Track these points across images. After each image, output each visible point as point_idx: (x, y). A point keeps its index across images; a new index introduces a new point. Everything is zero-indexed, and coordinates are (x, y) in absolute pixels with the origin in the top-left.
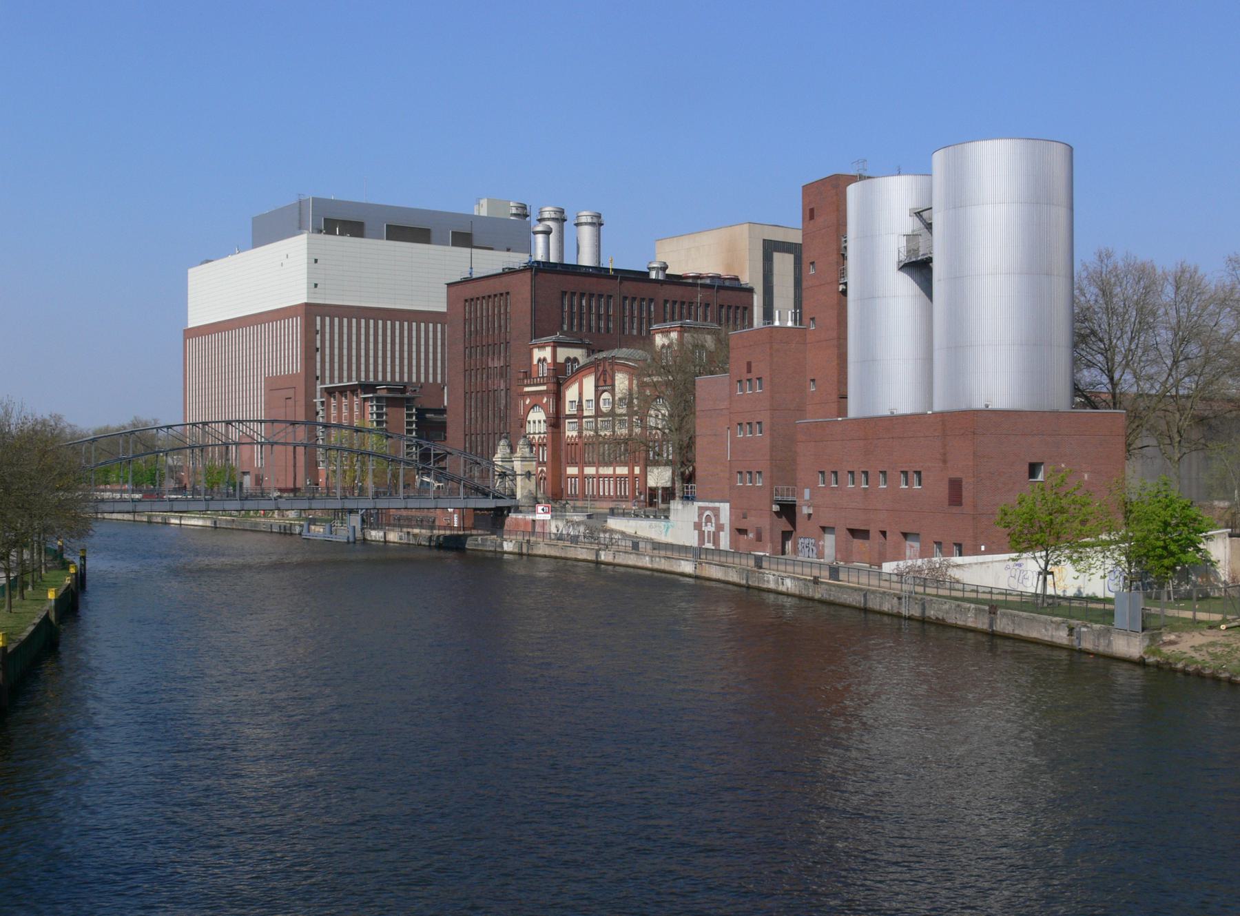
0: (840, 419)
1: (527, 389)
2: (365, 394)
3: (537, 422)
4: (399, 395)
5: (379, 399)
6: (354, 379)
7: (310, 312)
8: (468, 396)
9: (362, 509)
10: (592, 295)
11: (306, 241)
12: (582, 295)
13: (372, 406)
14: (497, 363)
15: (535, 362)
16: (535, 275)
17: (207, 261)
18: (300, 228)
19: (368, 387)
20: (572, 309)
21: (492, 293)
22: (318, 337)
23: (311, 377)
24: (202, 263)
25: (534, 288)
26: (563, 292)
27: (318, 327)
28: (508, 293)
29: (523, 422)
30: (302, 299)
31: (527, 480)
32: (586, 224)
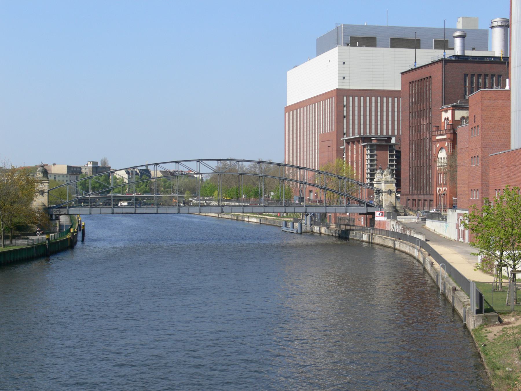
0: (501, 153)
1: (438, 138)
2: (364, 143)
3: (443, 158)
4: (384, 143)
5: (372, 146)
6: (356, 134)
7: (340, 93)
8: (411, 143)
9: (311, 213)
10: (486, 76)
11: (337, 52)
12: (479, 76)
13: (367, 150)
14: (425, 122)
15: (443, 120)
16: (445, 64)
17: (296, 66)
18: (337, 44)
19: (366, 139)
20: (472, 85)
21: (423, 77)
22: (345, 109)
23: (340, 132)
24: (294, 68)
25: (444, 73)
26: (465, 74)
27: (345, 103)
28: (430, 77)
29: (436, 158)
30: (336, 86)
31: (389, 195)
32: (497, 26)
